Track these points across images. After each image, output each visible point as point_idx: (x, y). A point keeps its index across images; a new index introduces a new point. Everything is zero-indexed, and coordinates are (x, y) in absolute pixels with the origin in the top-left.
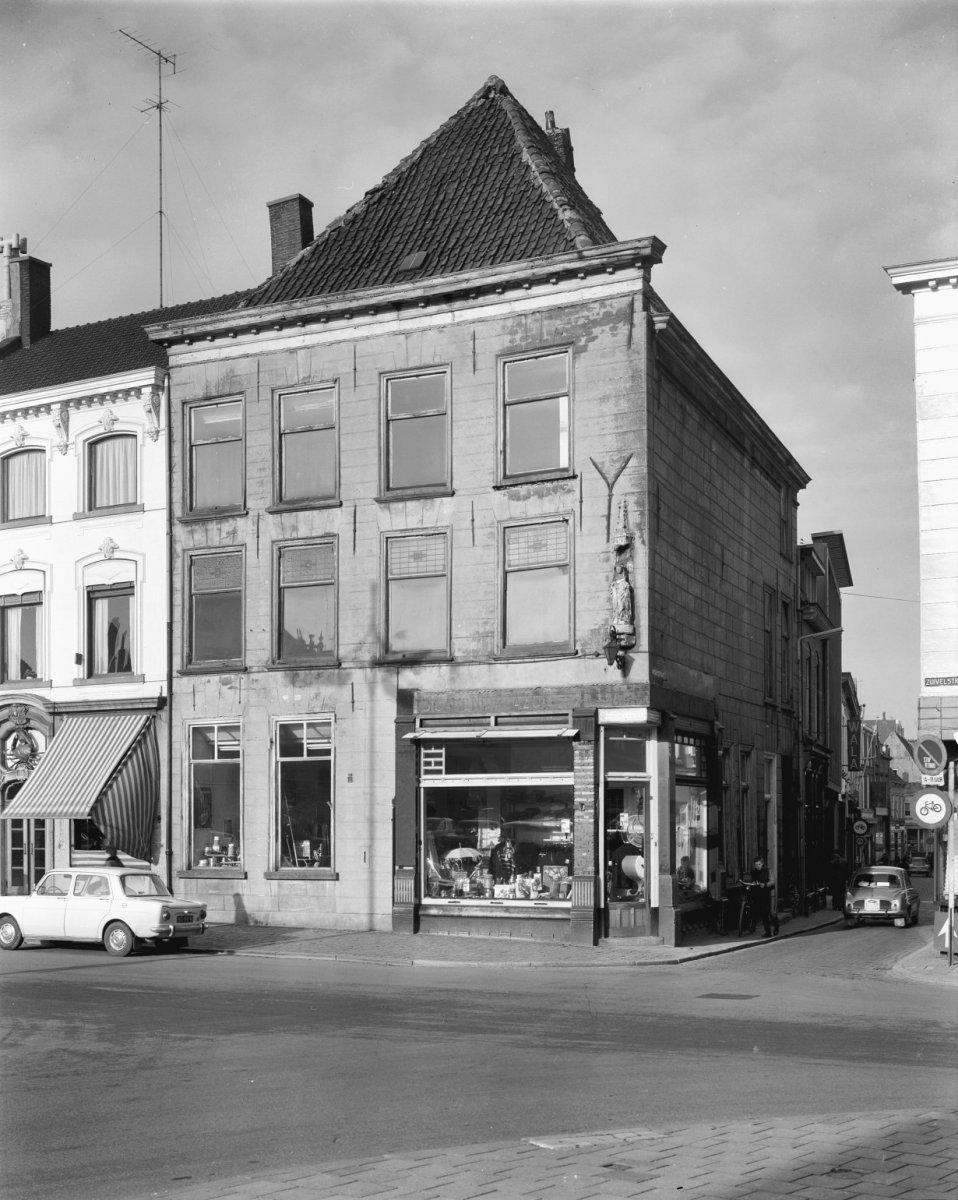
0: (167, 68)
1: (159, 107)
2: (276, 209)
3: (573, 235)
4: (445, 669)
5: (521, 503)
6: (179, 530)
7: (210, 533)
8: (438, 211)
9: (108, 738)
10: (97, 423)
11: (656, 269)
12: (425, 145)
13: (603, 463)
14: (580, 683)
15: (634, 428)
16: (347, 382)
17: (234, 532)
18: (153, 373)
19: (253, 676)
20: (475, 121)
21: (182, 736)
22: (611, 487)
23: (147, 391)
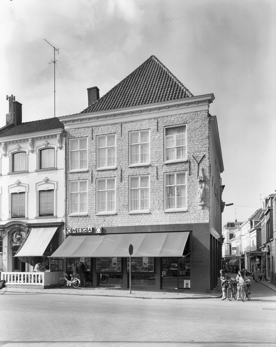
0: (56, 52)
1: (54, 62)
2: (89, 90)
10: (43, 145)
11: (211, 105)
23: (58, 136)
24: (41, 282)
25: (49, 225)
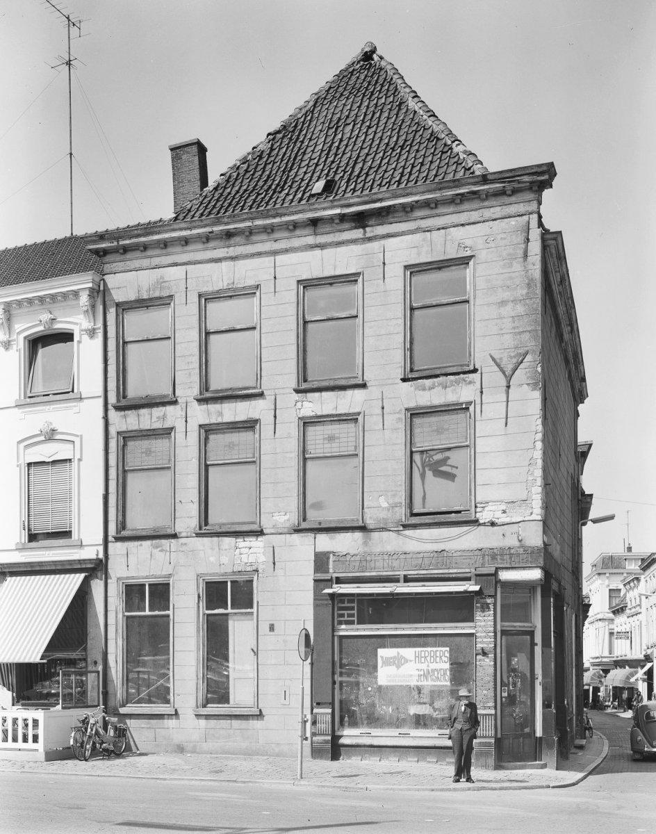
0: (74, 30)
1: (69, 63)
3: (470, 165)
4: (358, 535)
5: (427, 393)
6: (112, 414)
7: (141, 418)
8: (338, 148)
9: (40, 596)
11: (547, 194)
12: (316, 97)
13: (501, 359)
14: (480, 546)
15: (529, 329)
16: (267, 288)
17: (164, 417)
18: (91, 278)
19: (182, 541)
20: (358, 78)
21: (115, 590)
22: (509, 379)
23: (84, 299)
24: (35, 738)
25: (59, 567)
